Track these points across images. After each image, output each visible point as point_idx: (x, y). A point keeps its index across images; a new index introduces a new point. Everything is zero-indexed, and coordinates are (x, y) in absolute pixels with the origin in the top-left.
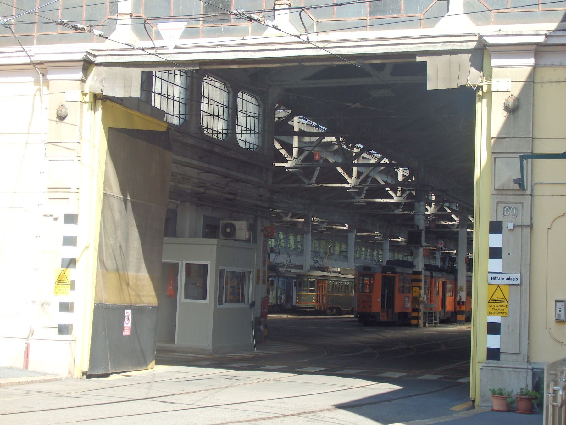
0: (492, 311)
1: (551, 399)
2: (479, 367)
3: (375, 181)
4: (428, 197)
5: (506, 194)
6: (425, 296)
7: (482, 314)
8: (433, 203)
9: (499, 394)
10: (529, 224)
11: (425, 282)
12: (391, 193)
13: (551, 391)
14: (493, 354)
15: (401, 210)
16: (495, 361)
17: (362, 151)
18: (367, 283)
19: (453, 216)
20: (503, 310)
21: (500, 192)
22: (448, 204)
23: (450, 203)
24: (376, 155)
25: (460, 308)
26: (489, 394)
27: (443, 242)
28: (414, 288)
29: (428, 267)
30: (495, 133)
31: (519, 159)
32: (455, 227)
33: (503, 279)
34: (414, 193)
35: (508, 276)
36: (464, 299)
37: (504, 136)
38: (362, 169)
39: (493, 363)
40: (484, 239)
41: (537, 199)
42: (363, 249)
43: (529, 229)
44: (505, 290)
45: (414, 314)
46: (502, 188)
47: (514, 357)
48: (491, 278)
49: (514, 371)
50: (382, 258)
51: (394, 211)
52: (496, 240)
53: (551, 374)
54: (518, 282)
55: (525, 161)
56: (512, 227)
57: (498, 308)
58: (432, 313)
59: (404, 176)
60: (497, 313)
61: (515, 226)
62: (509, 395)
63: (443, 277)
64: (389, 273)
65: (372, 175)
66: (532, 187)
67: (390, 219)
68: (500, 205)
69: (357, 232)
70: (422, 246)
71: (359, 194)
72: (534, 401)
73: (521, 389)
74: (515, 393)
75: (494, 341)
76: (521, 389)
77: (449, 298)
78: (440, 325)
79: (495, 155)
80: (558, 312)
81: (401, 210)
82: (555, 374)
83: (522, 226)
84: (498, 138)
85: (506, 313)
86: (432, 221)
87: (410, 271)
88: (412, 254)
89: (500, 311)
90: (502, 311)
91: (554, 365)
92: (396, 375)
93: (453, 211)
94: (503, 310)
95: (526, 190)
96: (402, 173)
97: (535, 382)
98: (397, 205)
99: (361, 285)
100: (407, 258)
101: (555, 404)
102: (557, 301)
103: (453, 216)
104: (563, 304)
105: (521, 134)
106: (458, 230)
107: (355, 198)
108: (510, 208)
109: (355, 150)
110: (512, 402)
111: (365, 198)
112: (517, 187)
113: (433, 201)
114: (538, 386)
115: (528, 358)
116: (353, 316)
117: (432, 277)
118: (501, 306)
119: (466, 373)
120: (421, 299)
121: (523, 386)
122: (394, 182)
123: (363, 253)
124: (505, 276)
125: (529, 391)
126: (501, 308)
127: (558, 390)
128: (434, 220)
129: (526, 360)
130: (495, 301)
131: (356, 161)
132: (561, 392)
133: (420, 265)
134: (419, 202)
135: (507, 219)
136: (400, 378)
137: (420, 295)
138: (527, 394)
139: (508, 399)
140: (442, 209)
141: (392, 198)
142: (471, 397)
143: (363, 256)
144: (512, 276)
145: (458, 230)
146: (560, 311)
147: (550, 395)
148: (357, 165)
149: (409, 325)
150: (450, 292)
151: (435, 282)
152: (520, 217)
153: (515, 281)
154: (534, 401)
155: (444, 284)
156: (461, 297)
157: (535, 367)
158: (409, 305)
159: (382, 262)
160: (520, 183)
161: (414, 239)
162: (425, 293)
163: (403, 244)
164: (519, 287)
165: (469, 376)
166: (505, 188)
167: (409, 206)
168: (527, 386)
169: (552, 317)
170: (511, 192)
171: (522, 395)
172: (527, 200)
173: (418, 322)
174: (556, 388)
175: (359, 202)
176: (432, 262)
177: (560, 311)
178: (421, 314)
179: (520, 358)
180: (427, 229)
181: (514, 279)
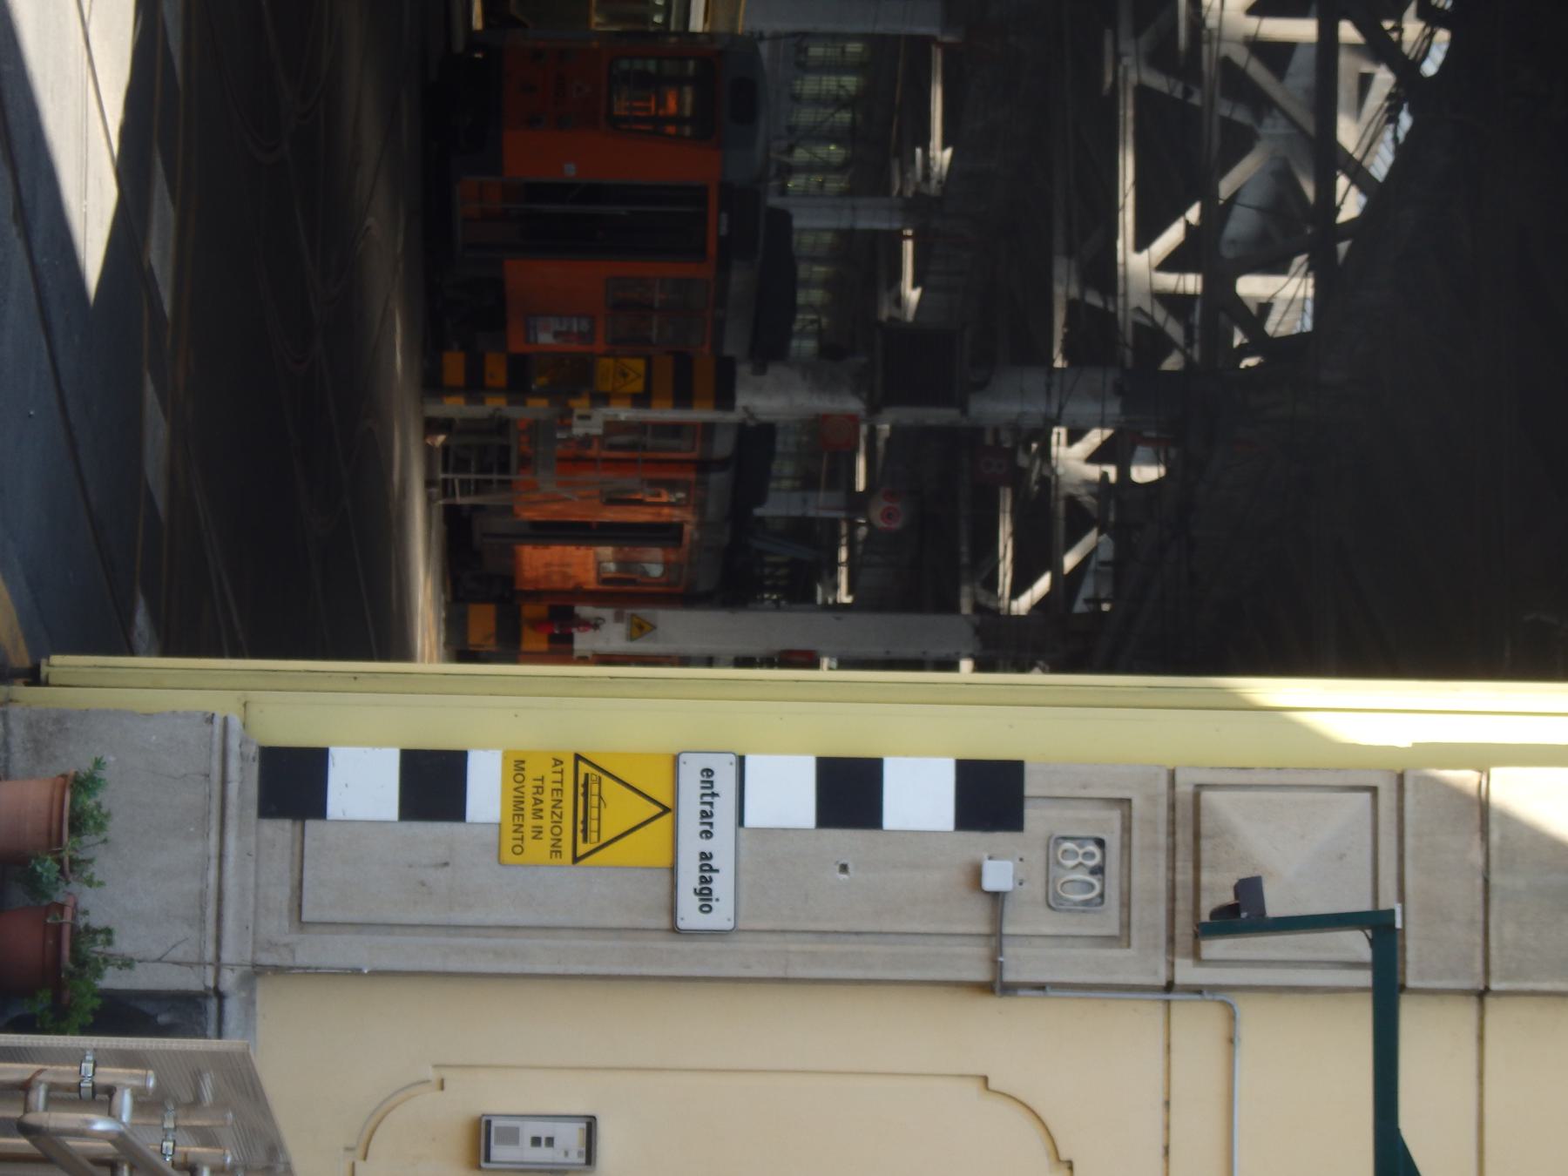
0: (531, 773)
1: (64, 1073)
2: (223, 704)
3: (1238, 143)
4: (1147, 441)
5: (1172, 851)
6: (595, 428)
7: (508, 719)
8: (1112, 471)
9: (77, 810)
10: (1009, 976)
11: (676, 429)
12: (1174, 235)
13: (109, 1075)
14: (294, 782)
15: (1074, 291)
16: (253, 791)
17: (1406, 68)
18: (661, 103)
19: (1043, 585)
20: (538, 832)
21: (1187, 816)
22: (1107, 553)
23: (1118, 565)
24: (1388, 135)
25: (537, 624)
26: (77, 760)
27: (897, 525)
28: (639, 365)
29: (757, 439)
30: (1520, 794)
31: (1366, 906)
32: (983, 598)
33: (707, 834)
34: (1173, 363)
35: (724, 860)
36: (583, 641)
37: (1495, 837)
38: (1302, 73)
39: (244, 783)
40: (925, 731)
41: (1144, 1017)
42: (850, 82)
43: (981, 974)
44: (648, 846)
45: (496, 371)
46: (1206, 825)
47: (281, 895)
48: (708, 772)
49: (202, 895)
50: (805, 194)
51: (1070, 253)
52: (919, 796)
53: (197, 1076)
54: (690, 914)
55: (1357, 944)
56: (991, 882)
57: (547, 806)
58: (505, 467)
59: (1266, 307)
60: (518, 804)
61: (997, 897)
62: (73, 868)
63: (700, 525)
64: (720, 224)
65: (1272, 129)
66: (1216, 989)
67: (1025, 226)
68: (1115, 816)
69: (948, 50)
70: (874, 409)
71: (1162, 56)
72: (45, 997)
73: (108, 931)
74: (87, 897)
75: (363, 785)
76: (108, 931)
77: (589, 563)
78: (438, 514)
79: (1392, 791)
80: (529, 1129)
81: (1074, 291)
82: (197, 1100)
83: (996, 937)
84: (1482, 809)
85: (519, 849)
86: (1017, 458)
87: (735, 344)
88: (830, 351)
89: (529, 822)
90: (528, 832)
91: (244, 1084)
92: (159, 256)
93: (1066, 586)
94: (538, 832)
95: (1196, 955)
96: (1284, 295)
97: (146, 1007)
98: (1103, 272)
99: (652, 66)
100: (803, 334)
101: (39, 1096)
102: (591, 1124)
103: (1043, 585)
104: (576, 1157)
105: (1504, 931)
106: (966, 607)
107: (1137, 33)
108: (1098, 871)
109: (1412, 29)
110: (33, 883)
111: (1142, 92)
112: (1219, 891)
113: (1124, 473)
114: (125, 1015)
115: (278, 970)
116: (477, 23)
117: (704, 466)
118: (557, 824)
119: (181, 639)
120: (580, 406)
121: (123, 945)
122: (1228, 252)
123: (829, 83)
124: (722, 847)
125: (98, 973)
126: (546, 823)
127: (110, 1112)
128: (1017, 478)
129: (266, 959)
130: (583, 790)
131: (1348, 32)
132: (101, 1125)
133: (769, 399)
134: (1119, 390)
135: (1037, 857)
136: (147, 278)
137: (603, 399)
138: (81, 961)
139: (49, 861)
140: (1079, 522)
141: (1142, 243)
142: (56, 659)
143: (810, 85)
144: (722, 885)
145: (966, 607)
146: (536, 1141)
147: (88, 1067)
148: (1328, 42)
149: (432, 343)
150: (623, 564)
151: (672, 486)
152: (1049, 924)
153: (696, 901)
154: (45, 997)
155: (665, 534)
156: (594, 625)
157: (231, 1006)
158: (545, 338)
159: (783, 191)
160: (1243, 913)
161: (908, 365)
162: (613, 427)
163: (885, 312)
164: (664, 922)
165: (169, 648)
166: (1206, 845)
167: (1097, 334)
168: (127, 963)
169: (499, 1097)
170: (1184, 876)
171: (76, 933)
172: (1142, 962)
173: (453, 391)
174: (125, 1101)
175: (1117, 58)
176: (784, 468)
177: (536, 1141)
178: (494, 405)
179: (276, 926)
180: (967, 440)
181: (705, 894)
